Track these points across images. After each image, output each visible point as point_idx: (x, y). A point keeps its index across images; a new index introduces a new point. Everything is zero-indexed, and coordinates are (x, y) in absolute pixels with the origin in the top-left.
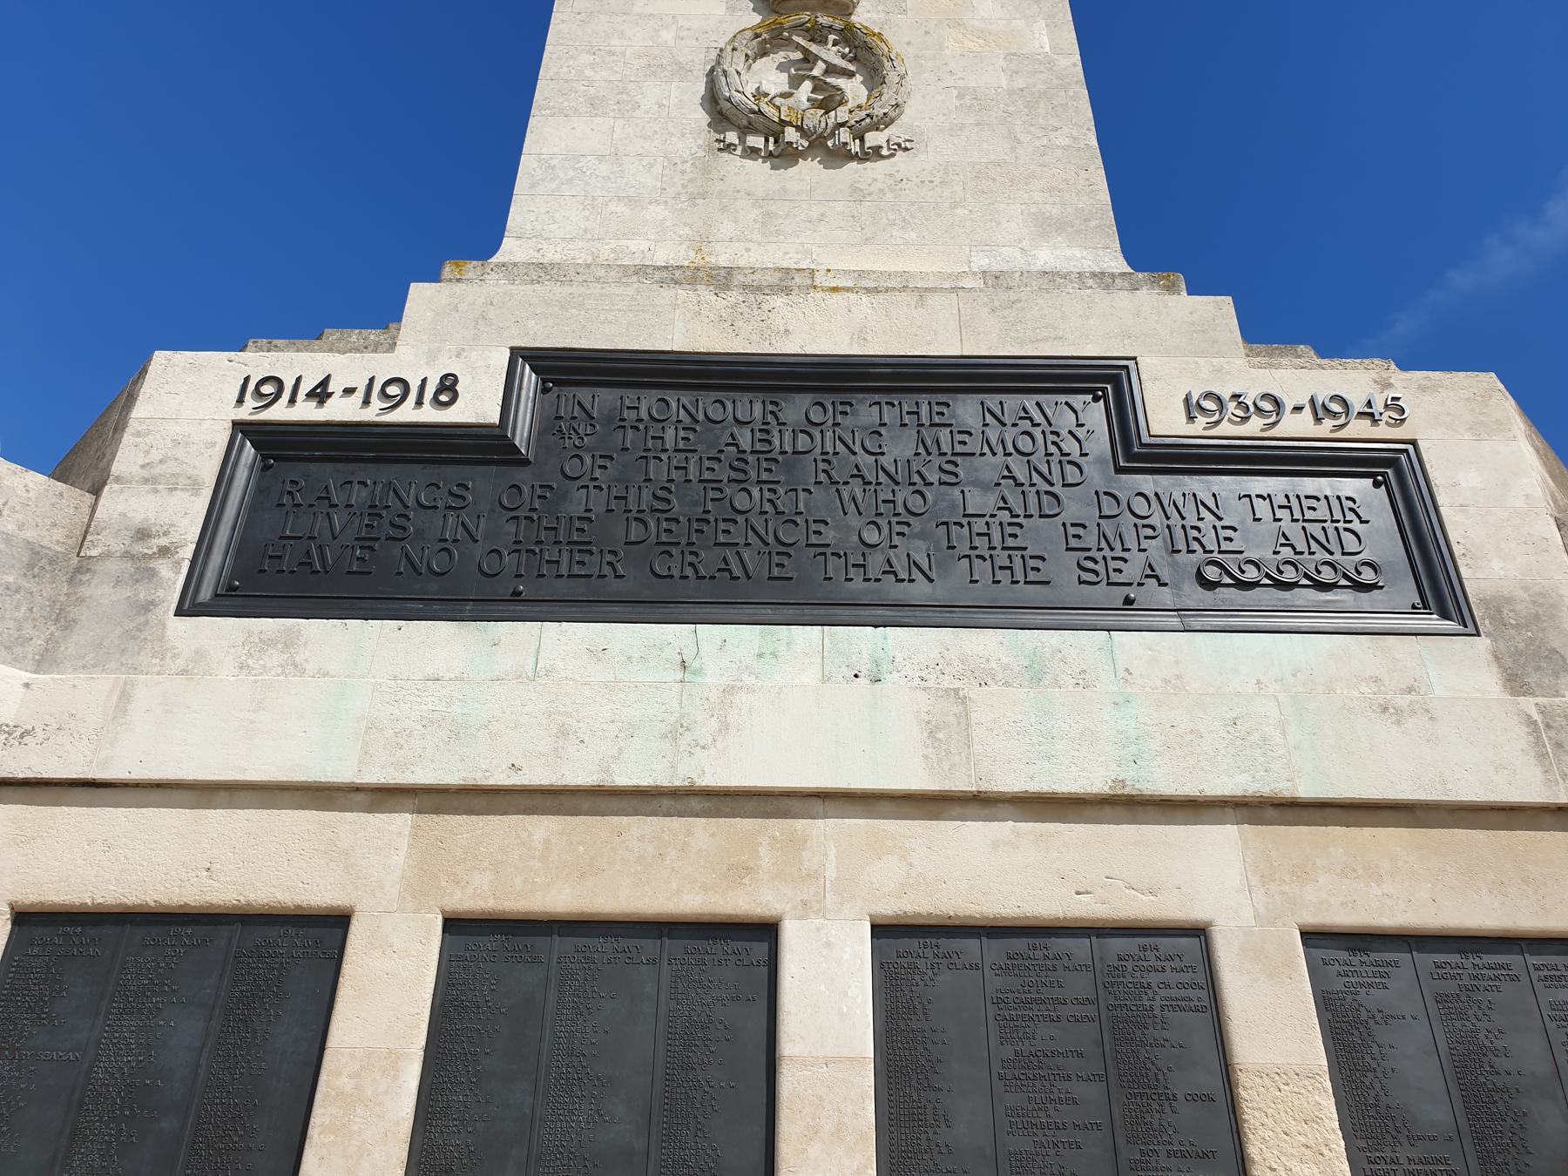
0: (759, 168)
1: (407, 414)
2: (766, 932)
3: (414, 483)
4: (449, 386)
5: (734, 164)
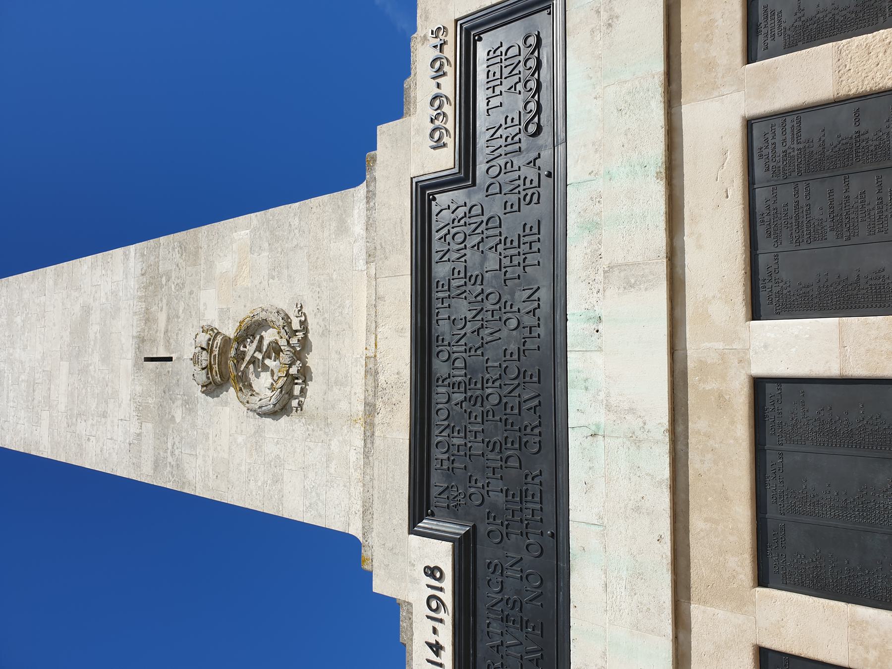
0: (311, 387)
1: (447, 597)
2: (759, 385)
3: (487, 595)
4: (431, 572)
5: (308, 402)
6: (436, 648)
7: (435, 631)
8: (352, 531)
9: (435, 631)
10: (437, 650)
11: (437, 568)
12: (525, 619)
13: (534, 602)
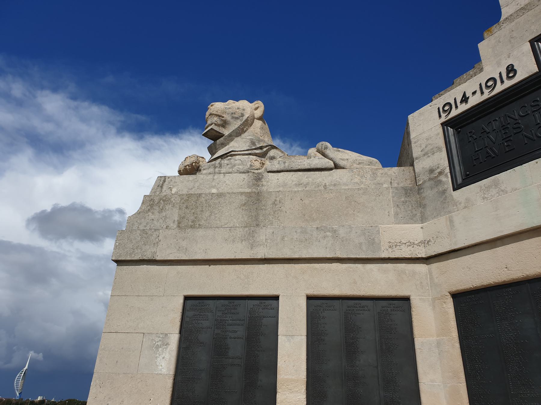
1: (499, 88)
4: (511, 70)
6: (465, 99)
7: (474, 93)
8: (503, 11)
9: (474, 93)
10: (464, 100)
11: (515, 72)
12: (511, 138)
13: (525, 139)
